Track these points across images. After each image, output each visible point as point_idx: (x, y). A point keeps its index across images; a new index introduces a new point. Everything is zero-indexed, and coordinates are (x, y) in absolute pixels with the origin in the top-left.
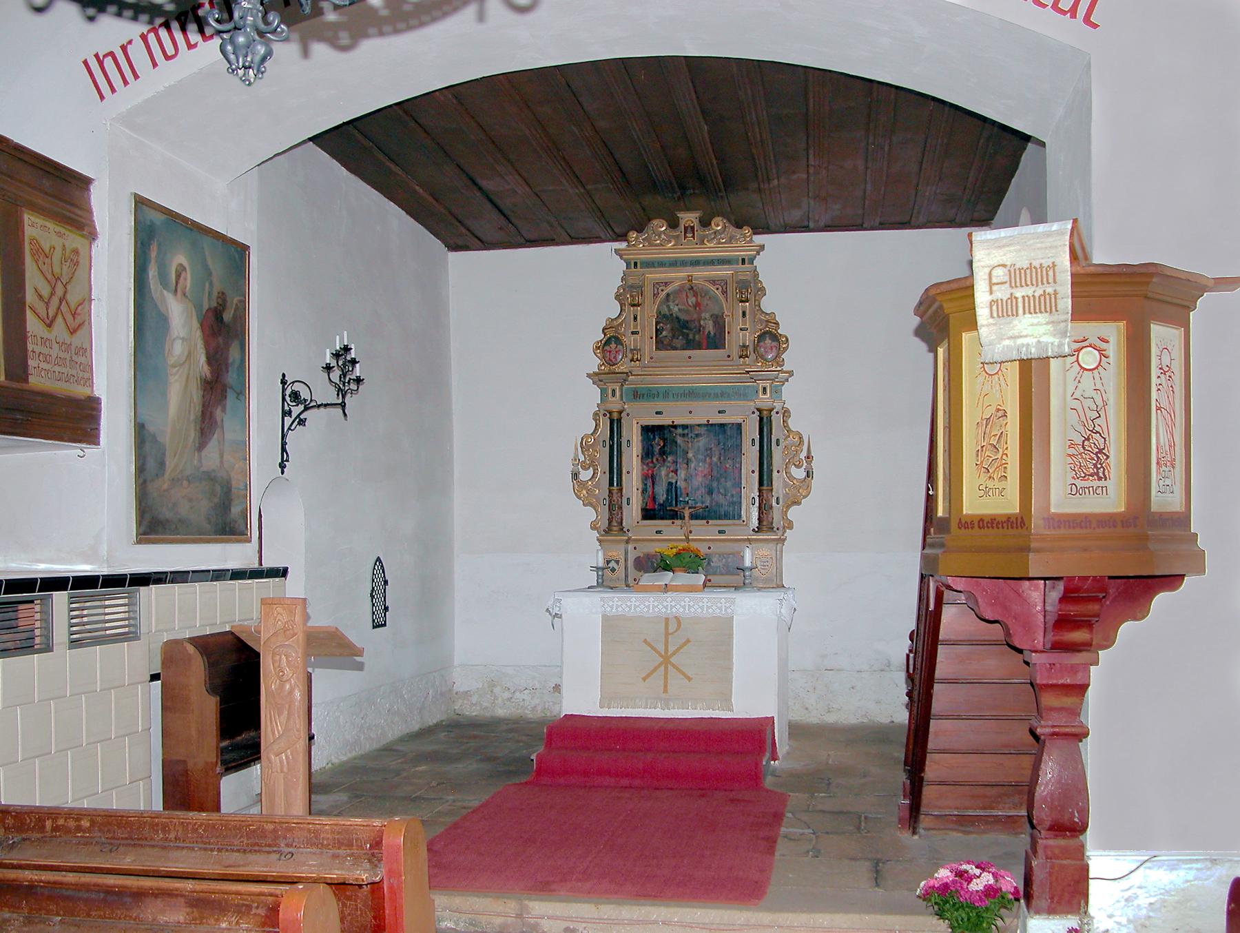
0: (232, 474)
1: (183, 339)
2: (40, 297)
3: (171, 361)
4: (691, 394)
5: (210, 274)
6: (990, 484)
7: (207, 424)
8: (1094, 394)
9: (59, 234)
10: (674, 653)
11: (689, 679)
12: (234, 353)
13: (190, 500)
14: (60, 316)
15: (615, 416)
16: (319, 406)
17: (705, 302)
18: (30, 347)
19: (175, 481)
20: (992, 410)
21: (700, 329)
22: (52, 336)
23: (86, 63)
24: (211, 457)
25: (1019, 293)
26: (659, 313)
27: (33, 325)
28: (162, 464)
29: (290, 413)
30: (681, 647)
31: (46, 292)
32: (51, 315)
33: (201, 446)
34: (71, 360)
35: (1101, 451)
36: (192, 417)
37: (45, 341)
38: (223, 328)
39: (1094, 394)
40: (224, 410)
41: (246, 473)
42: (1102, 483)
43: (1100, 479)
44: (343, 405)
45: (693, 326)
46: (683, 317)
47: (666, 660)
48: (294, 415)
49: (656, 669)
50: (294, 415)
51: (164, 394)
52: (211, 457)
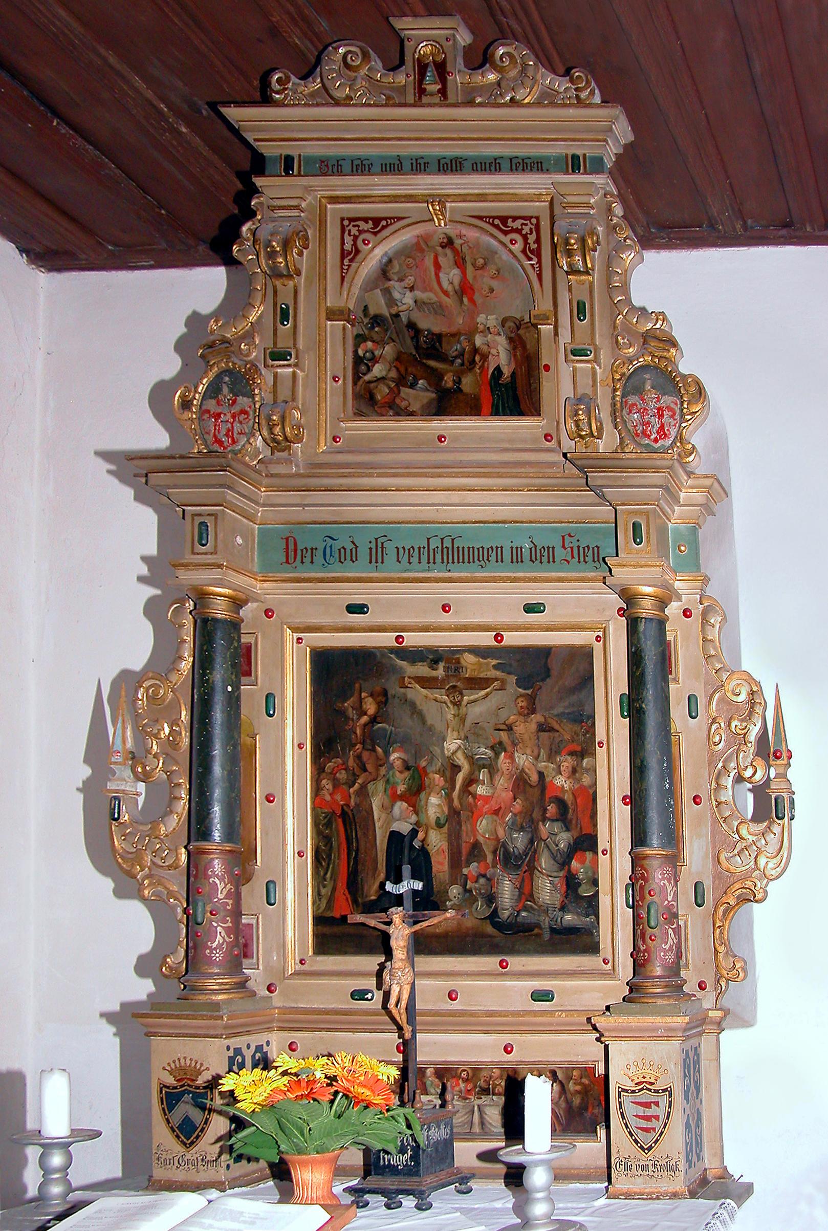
4: (450, 553)
15: (646, 609)
17: (484, 281)
21: (474, 358)
45: (453, 350)
46: (427, 323)
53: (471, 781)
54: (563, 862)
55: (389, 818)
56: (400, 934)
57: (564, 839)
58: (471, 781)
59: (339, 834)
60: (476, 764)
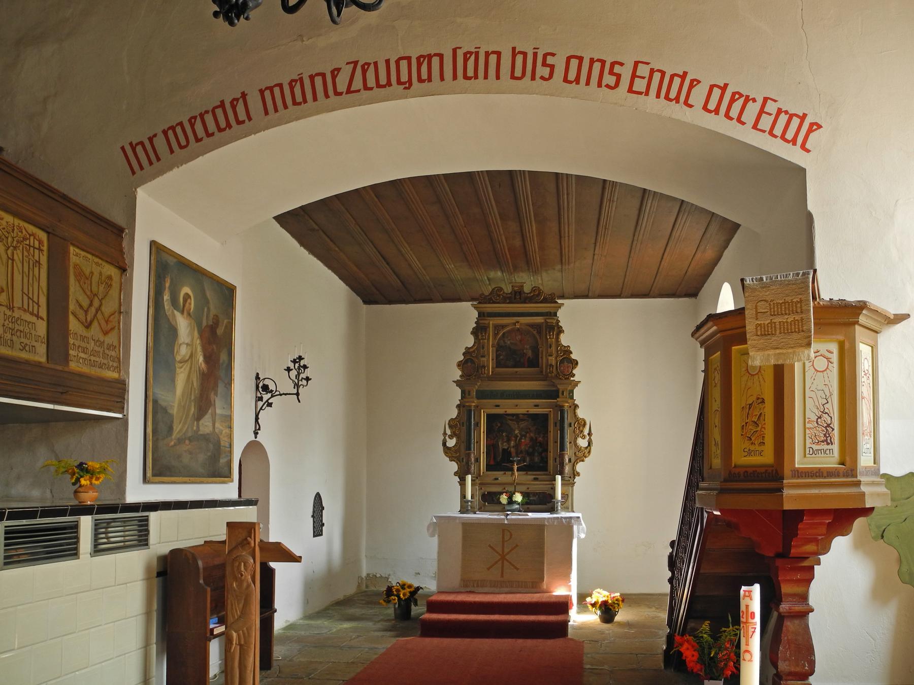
0: (221, 437)
1: (187, 344)
2: (81, 307)
3: (178, 358)
5: (208, 302)
6: (752, 448)
7: (203, 405)
8: (824, 387)
9: (97, 264)
10: (508, 553)
11: (517, 569)
12: (223, 357)
13: (191, 453)
14: (96, 321)
16: (281, 395)
18: (71, 341)
19: (180, 441)
20: (754, 398)
22: (89, 335)
23: (123, 148)
24: (206, 426)
25: (777, 320)
26: (498, 344)
27: (74, 325)
28: (171, 429)
29: (261, 399)
30: (512, 549)
31: (85, 304)
32: (89, 319)
33: (200, 415)
34: (104, 353)
35: (828, 425)
36: (193, 398)
37: (83, 338)
38: (217, 340)
39: (824, 387)
40: (216, 394)
41: (230, 437)
42: (830, 447)
43: (828, 444)
44: (298, 394)
47: (503, 558)
48: (264, 400)
49: (496, 562)
50: (264, 400)
51: (173, 380)
52: (206, 426)
53: (521, 439)
54: (540, 454)
55: (503, 445)
56: (516, 467)
57: (540, 450)
58: (521, 439)
59: (491, 449)
60: (522, 436)
